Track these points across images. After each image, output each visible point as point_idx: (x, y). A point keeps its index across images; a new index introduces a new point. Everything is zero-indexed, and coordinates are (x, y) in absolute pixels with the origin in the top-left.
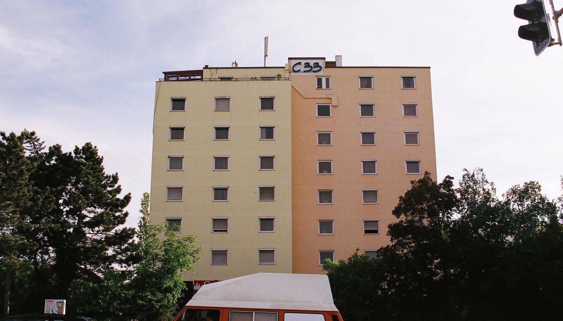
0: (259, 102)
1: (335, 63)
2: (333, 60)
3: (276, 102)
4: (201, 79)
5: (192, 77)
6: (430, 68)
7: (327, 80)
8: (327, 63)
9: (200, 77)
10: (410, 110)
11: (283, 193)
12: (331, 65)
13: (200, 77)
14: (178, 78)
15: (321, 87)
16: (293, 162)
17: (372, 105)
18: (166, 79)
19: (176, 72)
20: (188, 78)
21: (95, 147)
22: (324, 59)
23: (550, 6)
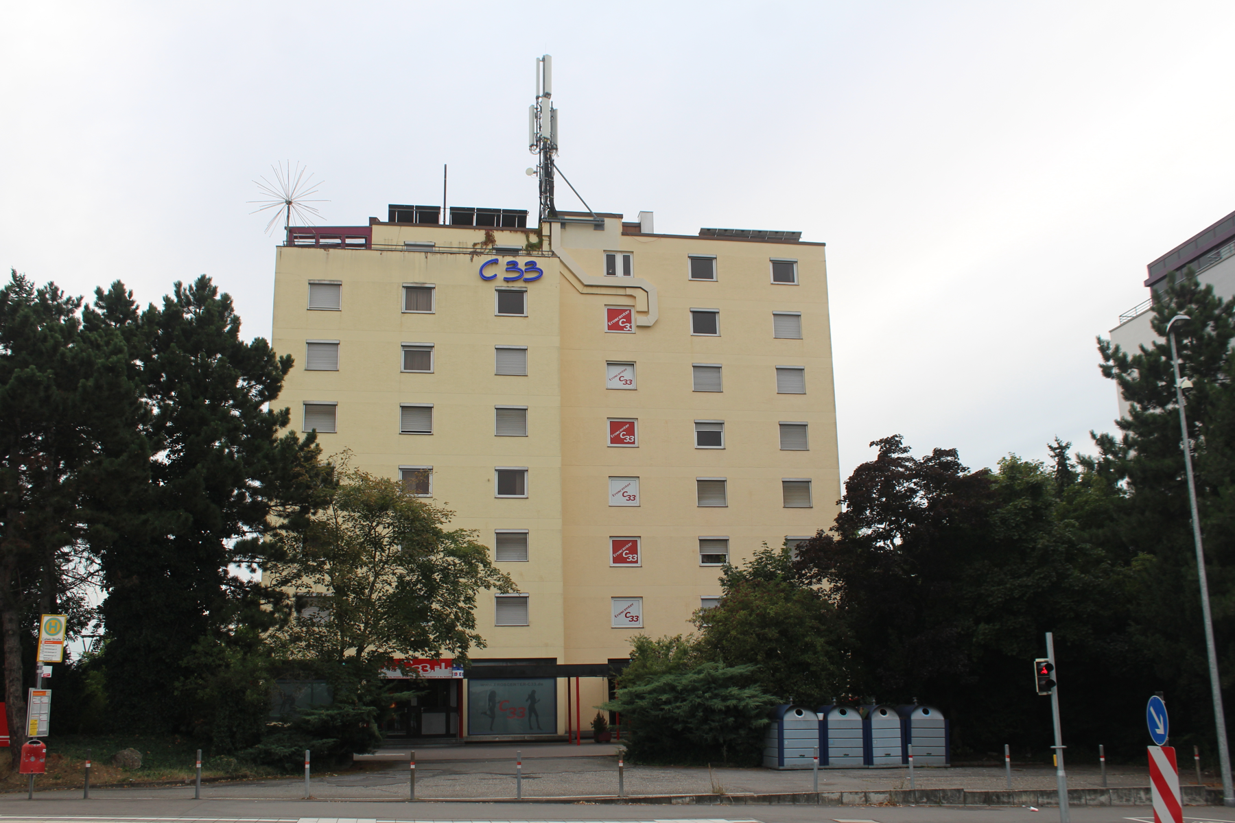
0: (495, 478)
1: (638, 226)
2: (636, 221)
3: (529, 480)
4: (368, 246)
5: (348, 241)
6: (824, 245)
7: (627, 260)
8: (625, 225)
9: (362, 241)
10: (790, 374)
11: (541, 360)
12: (632, 230)
13: (362, 241)
14: (317, 242)
15: (614, 273)
16: (552, 193)
17: (714, 313)
18: (290, 243)
19: (309, 228)
20: (338, 241)
21: (131, 294)
22: (621, 216)
23: (1035, 787)
